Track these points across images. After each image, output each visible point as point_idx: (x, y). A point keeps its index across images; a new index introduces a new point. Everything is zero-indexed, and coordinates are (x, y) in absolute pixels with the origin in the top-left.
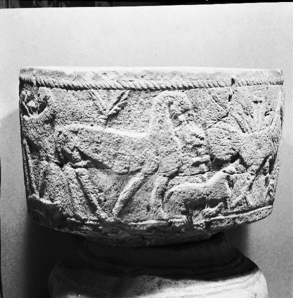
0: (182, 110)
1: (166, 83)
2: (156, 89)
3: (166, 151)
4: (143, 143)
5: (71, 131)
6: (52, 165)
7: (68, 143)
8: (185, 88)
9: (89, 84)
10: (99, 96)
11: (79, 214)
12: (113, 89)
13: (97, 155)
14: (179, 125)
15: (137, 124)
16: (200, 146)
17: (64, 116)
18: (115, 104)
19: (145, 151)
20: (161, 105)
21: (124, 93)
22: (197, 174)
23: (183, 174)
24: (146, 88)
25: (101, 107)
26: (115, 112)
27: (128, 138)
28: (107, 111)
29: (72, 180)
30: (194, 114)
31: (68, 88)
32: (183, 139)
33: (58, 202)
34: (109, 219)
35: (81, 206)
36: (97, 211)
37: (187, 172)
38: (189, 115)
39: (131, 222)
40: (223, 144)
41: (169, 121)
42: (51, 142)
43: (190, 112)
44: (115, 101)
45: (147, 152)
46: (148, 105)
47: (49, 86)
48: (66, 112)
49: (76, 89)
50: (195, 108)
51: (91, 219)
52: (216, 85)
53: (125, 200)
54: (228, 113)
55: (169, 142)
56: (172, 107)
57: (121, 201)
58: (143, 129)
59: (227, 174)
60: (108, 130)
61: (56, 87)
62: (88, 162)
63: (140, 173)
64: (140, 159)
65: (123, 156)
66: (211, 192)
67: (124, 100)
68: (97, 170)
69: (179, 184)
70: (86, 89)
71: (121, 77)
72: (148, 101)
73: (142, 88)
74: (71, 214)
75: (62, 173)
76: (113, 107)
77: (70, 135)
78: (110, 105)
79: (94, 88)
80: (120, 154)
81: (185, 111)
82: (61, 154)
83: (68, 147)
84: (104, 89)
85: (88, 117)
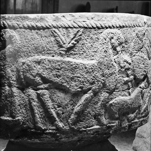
0: (119, 43)
1: (108, 23)
2: (103, 28)
3: (108, 73)
4: (93, 68)
5: (35, 61)
6: (15, 89)
7: (31, 71)
8: (121, 27)
9: (51, 25)
10: (59, 33)
11: (40, 125)
12: (71, 28)
13: (57, 79)
14: (117, 54)
15: (88, 54)
16: (128, 69)
17: (28, 50)
18: (72, 39)
19: (94, 74)
20: (106, 40)
21: (79, 30)
22: (126, 90)
23: (118, 90)
24: (96, 26)
25: (61, 41)
26: (72, 45)
27: (82, 65)
28: (67, 44)
29: (34, 99)
30: (126, 46)
31: (32, 28)
32: (119, 64)
33: (20, 118)
34: (65, 127)
35: (41, 119)
36: (56, 122)
37: (121, 88)
38: (123, 47)
39: (82, 128)
40: (141, 68)
41: (111, 51)
42: (14, 71)
43: (123, 45)
44: (72, 37)
45: (96, 75)
46: (97, 39)
47: (14, 28)
48: (29, 47)
49: (39, 28)
50: (126, 41)
51: (50, 129)
52: (138, 25)
53: (78, 111)
54: (143, 45)
55: (111, 67)
56: (113, 41)
57: (76, 113)
58: (93, 58)
59: (141, 89)
60: (67, 59)
61: (21, 28)
62: (49, 85)
63: (91, 91)
64: (91, 80)
65: (78, 79)
66: (133, 103)
67: (80, 36)
68: (56, 90)
69: (115, 98)
70: (48, 28)
71: (76, 19)
72: (96, 36)
73: (92, 26)
74: (32, 126)
75: (23, 95)
76: (71, 42)
77: (33, 64)
78: (68, 40)
79: (55, 27)
80: (76, 77)
81: (120, 44)
82: (23, 80)
83: (31, 74)
84: (64, 28)
85: (50, 50)
